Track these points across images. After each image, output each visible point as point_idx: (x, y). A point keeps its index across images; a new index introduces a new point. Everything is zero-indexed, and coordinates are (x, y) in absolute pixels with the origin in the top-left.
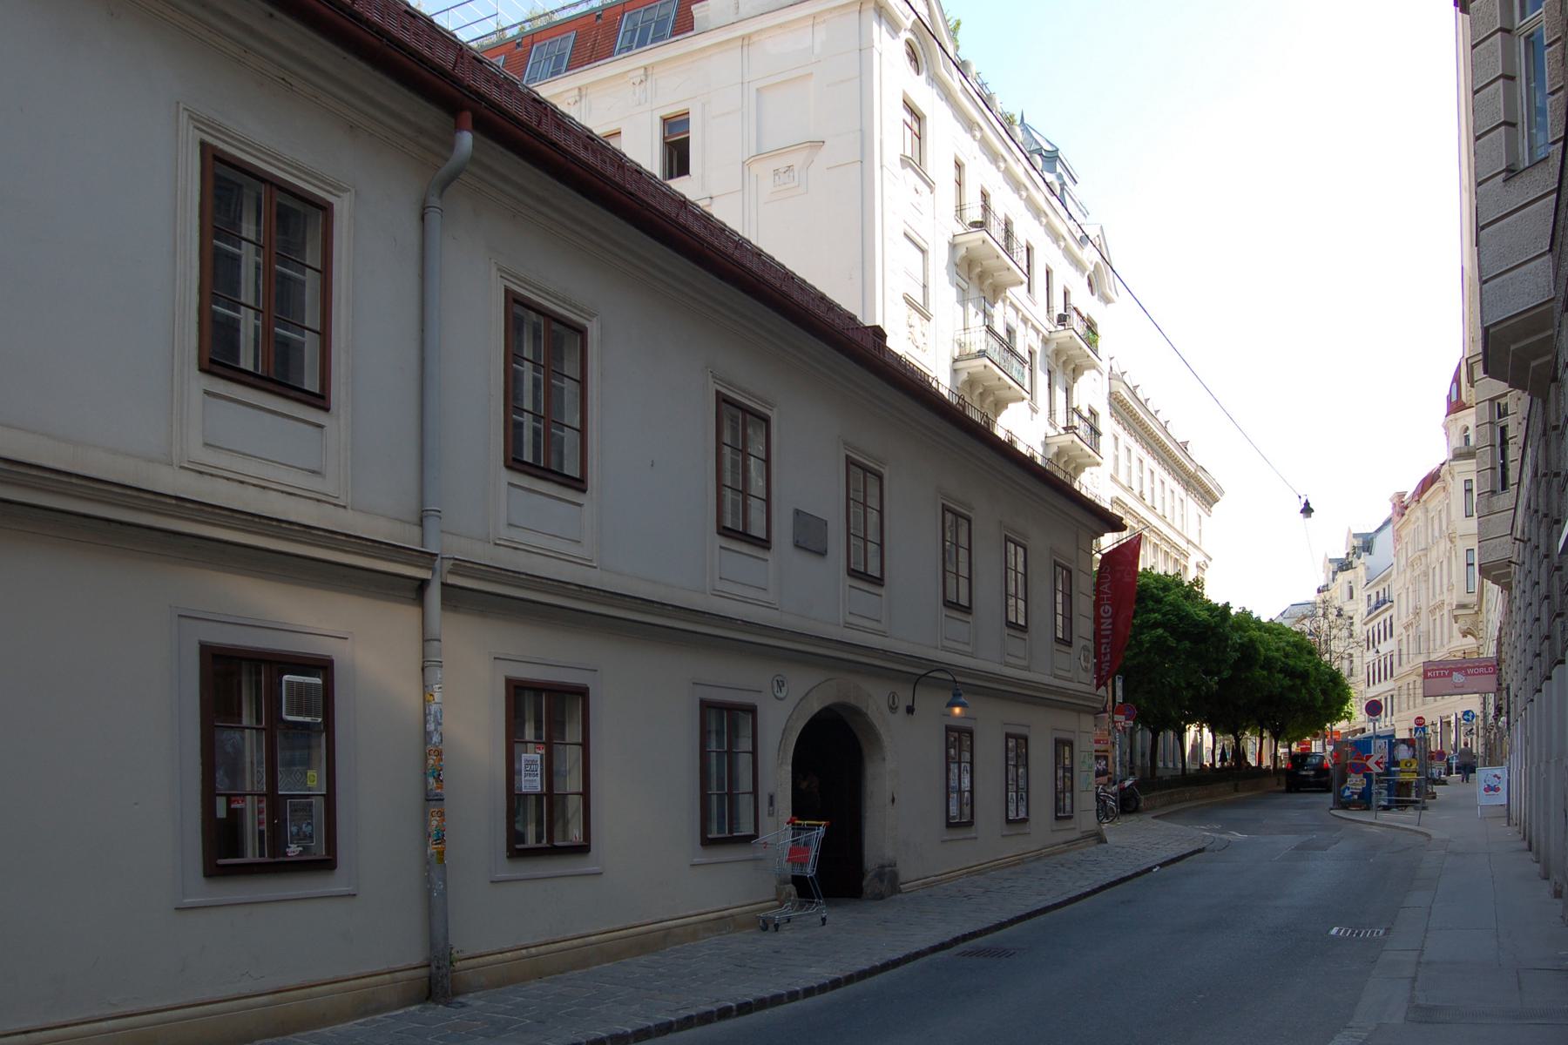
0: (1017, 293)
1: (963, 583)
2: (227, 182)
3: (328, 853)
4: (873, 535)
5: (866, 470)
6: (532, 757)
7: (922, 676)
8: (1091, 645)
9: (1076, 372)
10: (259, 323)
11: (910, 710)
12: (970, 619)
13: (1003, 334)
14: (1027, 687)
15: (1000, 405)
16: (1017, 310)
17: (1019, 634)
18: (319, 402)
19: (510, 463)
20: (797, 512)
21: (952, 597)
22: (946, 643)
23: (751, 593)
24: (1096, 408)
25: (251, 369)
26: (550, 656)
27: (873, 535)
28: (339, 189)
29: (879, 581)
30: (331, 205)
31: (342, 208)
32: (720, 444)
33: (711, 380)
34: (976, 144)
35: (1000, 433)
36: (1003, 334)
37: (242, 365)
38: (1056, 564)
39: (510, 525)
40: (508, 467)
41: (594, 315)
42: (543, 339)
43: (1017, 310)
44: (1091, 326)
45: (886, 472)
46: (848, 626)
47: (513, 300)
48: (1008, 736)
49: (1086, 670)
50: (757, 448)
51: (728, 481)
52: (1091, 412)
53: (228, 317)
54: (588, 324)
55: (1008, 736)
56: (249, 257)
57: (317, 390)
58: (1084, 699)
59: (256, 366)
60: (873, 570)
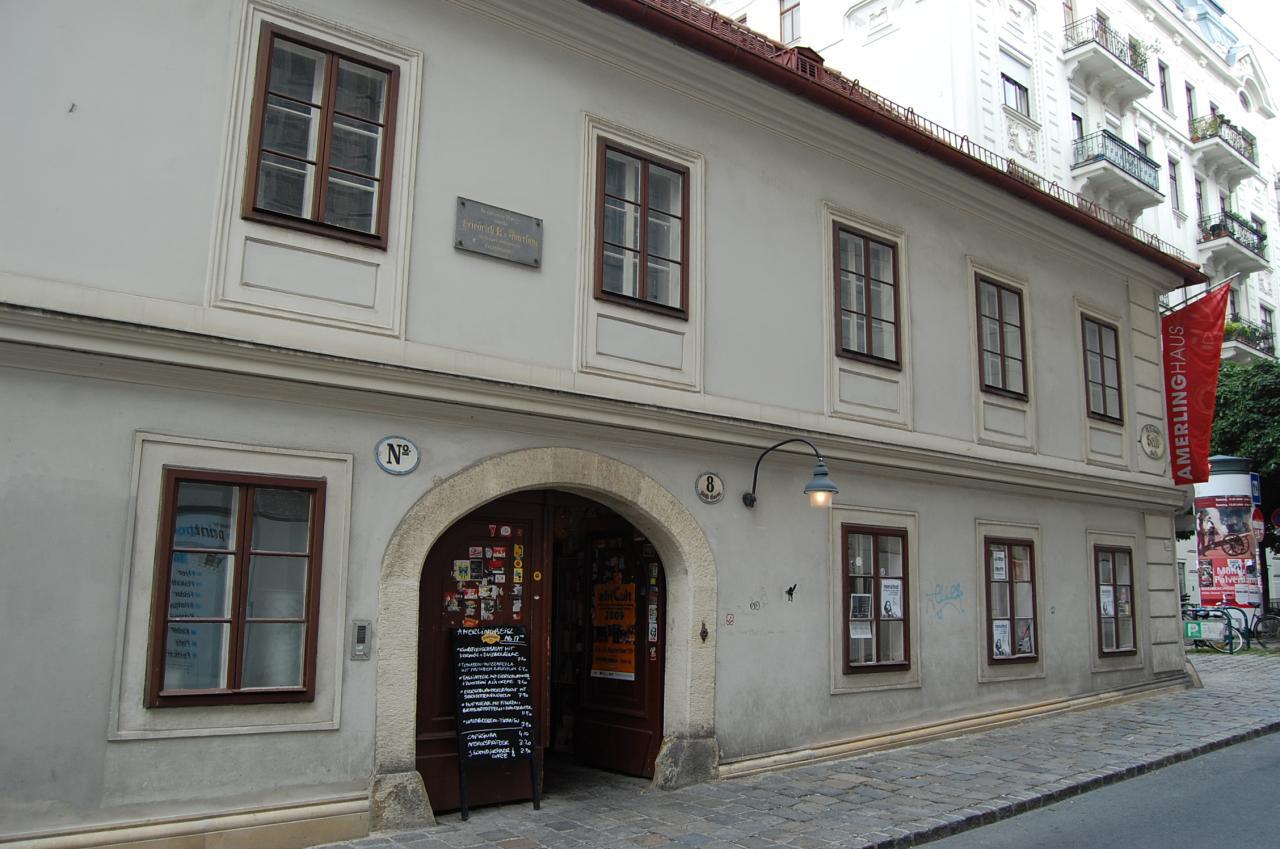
0: (1151, 103)
1: (1112, 395)
2: (612, 159)
3: (905, 659)
4: (1111, 381)
5: (1101, 324)
6: (1107, 592)
7: (770, 456)
8: (1162, 426)
9: (1233, 181)
10: (637, 261)
11: (749, 501)
12: (1025, 407)
13: (1137, 146)
14: (1021, 474)
15: (1135, 210)
16: (1152, 122)
17: (1018, 405)
18: (1119, 422)
19: (840, 352)
20: (462, 202)
21: (989, 381)
22: (1093, 457)
23: (667, 375)
24: (1261, 215)
25: (631, 295)
26: (877, 508)
27: (1111, 381)
28: (407, 55)
29: (895, 365)
30: (398, 68)
31: (696, 171)
32: (979, 316)
33: (824, 211)
34: (1180, 48)
35: (1138, 235)
36: (1137, 146)
37: (625, 293)
38: (1085, 318)
39: (599, 353)
40: (838, 355)
41: (902, 233)
42: (862, 258)
43: (1152, 122)
44: (1249, 140)
45: (901, 242)
46: (587, 370)
47: (839, 228)
48: (991, 542)
49: (1153, 456)
50: (1012, 317)
51: (988, 345)
52: (1255, 219)
53: (294, 173)
54: (898, 240)
55: (991, 542)
56: (630, 213)
57: (677, 305)
58: (1148, 493)
59: (634, 293)
60: (1113, 412)
